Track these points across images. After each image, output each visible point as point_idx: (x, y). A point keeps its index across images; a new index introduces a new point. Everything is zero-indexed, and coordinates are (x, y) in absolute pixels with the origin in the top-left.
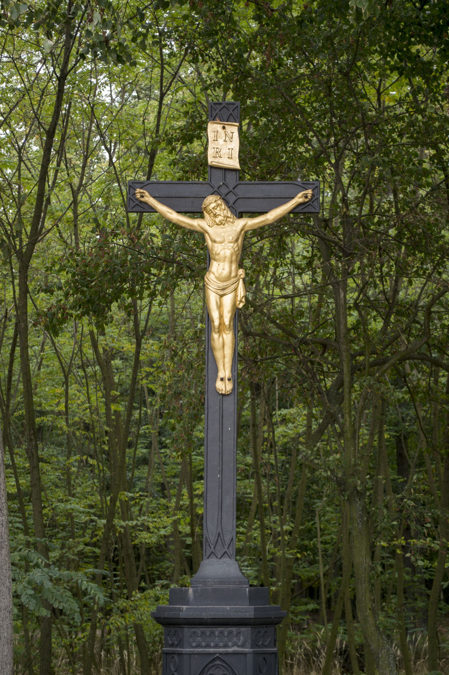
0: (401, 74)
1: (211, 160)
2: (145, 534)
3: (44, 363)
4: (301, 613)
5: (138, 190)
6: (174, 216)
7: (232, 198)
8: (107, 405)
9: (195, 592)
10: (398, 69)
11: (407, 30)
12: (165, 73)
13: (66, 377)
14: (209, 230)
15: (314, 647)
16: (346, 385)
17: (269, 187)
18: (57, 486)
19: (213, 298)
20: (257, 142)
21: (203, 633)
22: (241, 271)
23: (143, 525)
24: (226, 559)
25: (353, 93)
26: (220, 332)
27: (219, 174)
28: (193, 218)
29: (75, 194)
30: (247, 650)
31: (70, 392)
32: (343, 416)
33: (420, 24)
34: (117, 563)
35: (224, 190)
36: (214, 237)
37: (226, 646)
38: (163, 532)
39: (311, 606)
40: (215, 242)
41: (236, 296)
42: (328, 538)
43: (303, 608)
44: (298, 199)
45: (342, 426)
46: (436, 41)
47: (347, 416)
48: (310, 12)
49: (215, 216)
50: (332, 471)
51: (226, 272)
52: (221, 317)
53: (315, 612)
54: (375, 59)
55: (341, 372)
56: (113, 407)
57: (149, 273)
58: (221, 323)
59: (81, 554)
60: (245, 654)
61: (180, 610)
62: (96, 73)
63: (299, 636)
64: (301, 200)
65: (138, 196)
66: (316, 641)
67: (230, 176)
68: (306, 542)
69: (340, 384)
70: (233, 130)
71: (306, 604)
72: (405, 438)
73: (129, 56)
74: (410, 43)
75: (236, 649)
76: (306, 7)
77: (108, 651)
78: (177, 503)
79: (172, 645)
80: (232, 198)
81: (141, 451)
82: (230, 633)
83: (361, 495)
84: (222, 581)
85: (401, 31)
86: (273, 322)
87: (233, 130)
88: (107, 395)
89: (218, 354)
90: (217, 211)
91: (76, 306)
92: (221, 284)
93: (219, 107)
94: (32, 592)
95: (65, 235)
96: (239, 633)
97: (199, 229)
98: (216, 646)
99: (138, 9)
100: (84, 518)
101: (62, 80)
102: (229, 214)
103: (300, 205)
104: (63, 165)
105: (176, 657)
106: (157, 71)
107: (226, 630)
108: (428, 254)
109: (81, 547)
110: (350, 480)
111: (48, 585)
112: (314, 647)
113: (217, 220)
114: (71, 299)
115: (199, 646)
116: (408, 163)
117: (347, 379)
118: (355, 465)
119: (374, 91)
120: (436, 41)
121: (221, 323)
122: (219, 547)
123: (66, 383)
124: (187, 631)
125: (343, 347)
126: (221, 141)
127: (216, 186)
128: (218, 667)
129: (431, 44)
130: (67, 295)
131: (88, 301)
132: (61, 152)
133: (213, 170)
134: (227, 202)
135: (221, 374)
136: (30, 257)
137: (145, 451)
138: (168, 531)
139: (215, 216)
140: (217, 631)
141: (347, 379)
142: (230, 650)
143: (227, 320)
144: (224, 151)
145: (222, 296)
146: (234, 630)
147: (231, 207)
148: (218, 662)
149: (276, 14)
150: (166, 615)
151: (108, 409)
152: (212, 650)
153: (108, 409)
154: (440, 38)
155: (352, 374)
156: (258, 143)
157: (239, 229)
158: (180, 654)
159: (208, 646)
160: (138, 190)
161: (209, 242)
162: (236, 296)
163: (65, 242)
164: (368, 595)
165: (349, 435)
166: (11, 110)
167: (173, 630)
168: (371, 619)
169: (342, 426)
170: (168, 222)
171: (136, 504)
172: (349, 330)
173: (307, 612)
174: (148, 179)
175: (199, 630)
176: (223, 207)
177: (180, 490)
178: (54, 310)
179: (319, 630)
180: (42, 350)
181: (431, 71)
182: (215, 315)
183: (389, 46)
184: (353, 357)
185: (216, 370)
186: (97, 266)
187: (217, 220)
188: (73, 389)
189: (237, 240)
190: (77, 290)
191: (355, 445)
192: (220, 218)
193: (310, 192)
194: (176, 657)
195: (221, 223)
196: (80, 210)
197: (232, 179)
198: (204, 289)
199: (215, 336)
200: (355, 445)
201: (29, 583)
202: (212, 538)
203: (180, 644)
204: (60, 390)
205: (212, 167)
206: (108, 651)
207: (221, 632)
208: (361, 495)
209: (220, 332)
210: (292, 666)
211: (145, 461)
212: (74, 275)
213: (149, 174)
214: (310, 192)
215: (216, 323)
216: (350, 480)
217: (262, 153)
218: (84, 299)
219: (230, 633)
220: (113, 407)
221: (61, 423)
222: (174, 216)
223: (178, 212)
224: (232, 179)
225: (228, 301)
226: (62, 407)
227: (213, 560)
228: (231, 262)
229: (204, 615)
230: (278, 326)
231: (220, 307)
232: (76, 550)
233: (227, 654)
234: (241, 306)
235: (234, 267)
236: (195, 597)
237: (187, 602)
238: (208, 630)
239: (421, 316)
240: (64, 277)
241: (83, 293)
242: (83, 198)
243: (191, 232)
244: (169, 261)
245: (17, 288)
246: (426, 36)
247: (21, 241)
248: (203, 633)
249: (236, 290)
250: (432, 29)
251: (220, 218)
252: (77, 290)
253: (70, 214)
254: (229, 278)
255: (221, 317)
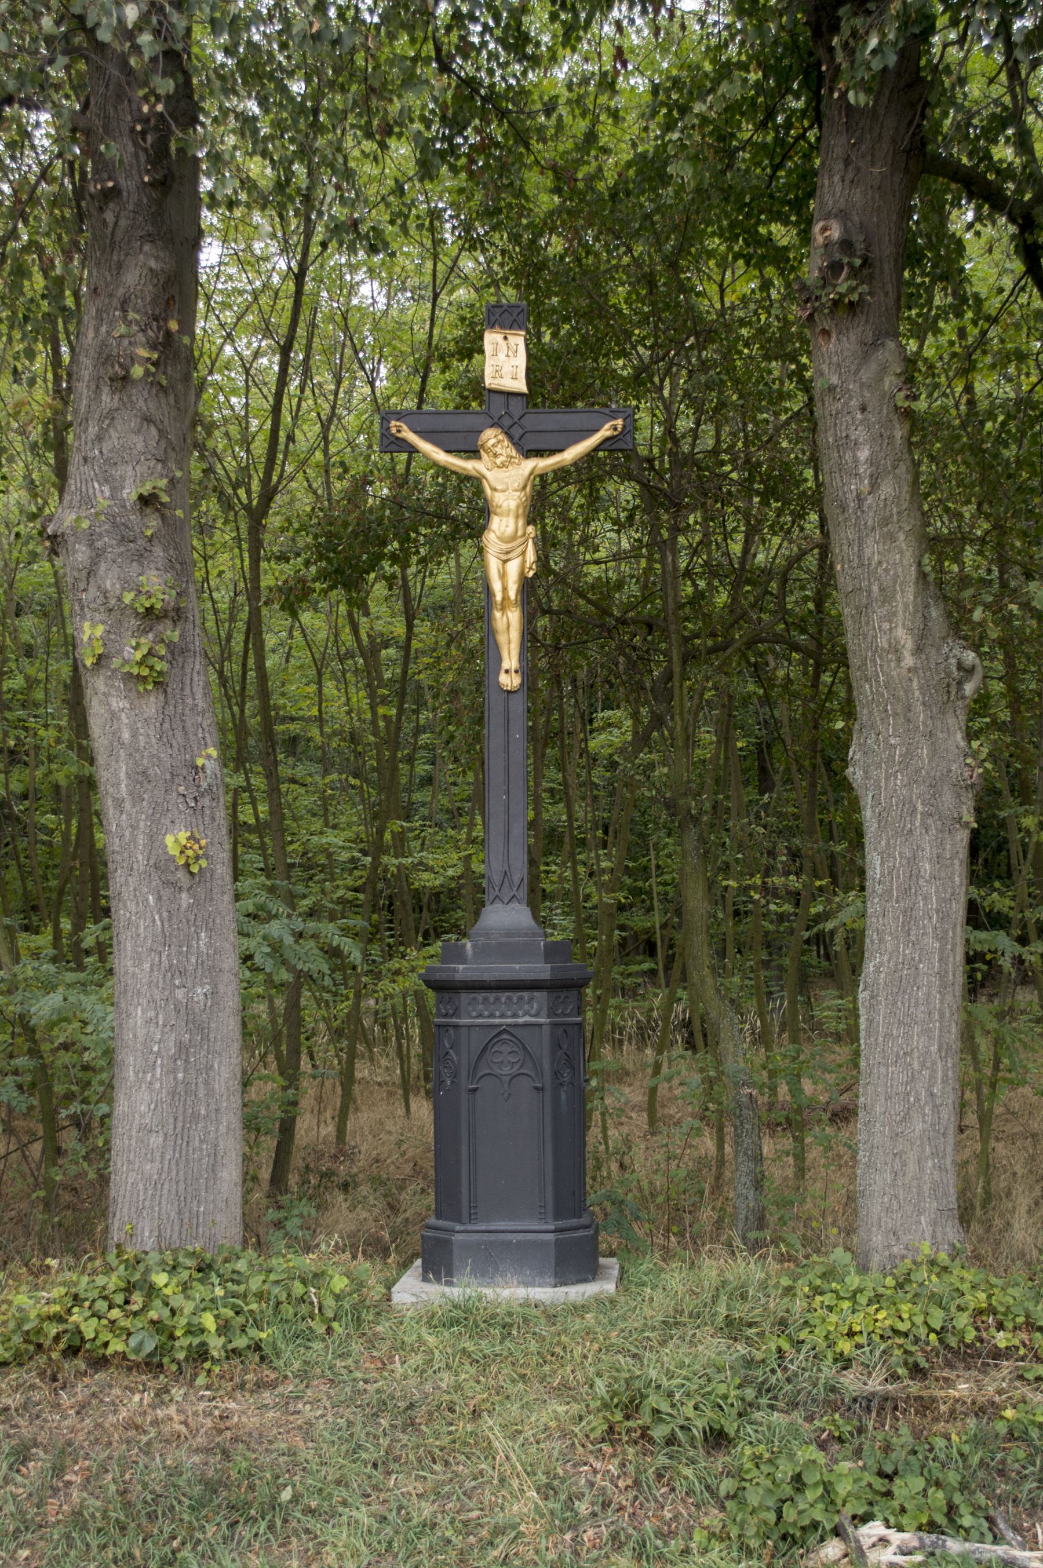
0: (748, 264)
1: (489, 382)
2: (425, 876)
3: (294, 652)
4: (637, 974)
5: (393, 423)
6: (441, 456)
7: (517, 432)
8: (373, 707)
9: (474, 947)
10: (743, 256)
11: (754, 204)
12: (440, 265)
13: (320, 674)
14: (488, 474)
15: (649, 1018)
16: (676, 677)
17: (566, 417)
18: (314, 815)
19: (493, 565)
20: (556, 356)
21: (486, 999)
22: (530, 529)
23: (421, 863)
24: (515, 905)
25: (685, 288)
26: (503, 609)
27: (501, 399)
28: (468, 458)
29: (325, 428)
30: (542, 1020)
31: (325, 691)
32: (672, 718)
33: (771, 196)
34: (392, 912)
35: (507, 422)
36: (494, 484)
37: (515, 1016)
38: (450, 872)
39: (646, 966)
40: (495, 490)
41: (524, 562)
42: (667, 877)
43: (635, 968)
44: (605, 432)
45: (671, 731)
46: (793, 218)
47: (677, 718)
48: (626, 182)
49: (496, 455)
50: (658, 792)
51: (510, 530)
52: (505, 589)
53: (653, 973)
54: (714, 243)
55: (670, 661)
56: (381, 711)
57: (419, 534)
58: (505, 598)
59: (341, 901)
60: (540, 1025)
61: (455, 970)
62: (353, 268)
63: (631, 1003)
64: (608, 433)
65: (394, 430)
66: (651, 1010)
67: (514, 402)
68: (640, 884)
69: (668, 676)
70: (518, 340)
71: (640, 963)
72: (769, 746)
73: (386, 245)
74: (759, 222)
75: (527, 1019)
76: (620, 175)
77: (384, 1026)
78: (469, 834)
79: (446, 1015)
80: (517, 432)
81: (422, 768)
82: (521, 998)
83: (696, 820)
84: (509, 933)
85: (746, 205)
86: (582, 595)
87: (518, 340)
88: (372, 696)
89: (502, 639)
90: (498, 450)
91: (322, 576)
92: (505, 547)
93: (499, 311)
94: (268, 950)
95: (315, 485)
96: (531, 999)
97: (474, 473)
98: (502, 1016)
99: (396, 180)
100: (345, 856)
101: (299, 278)
102: (514, 453)
103: (607, 439)
104: (308, 392)
105: (451, 1031)
106: (429, 265)
107: (515, 996)
108: (786, 503)
109: (341, 892)
110: (682, 802)
111: (289, 940)
112: (649, 1018)
113: (498, 461)
114: (313, 569)
115: (480, 1016)
116: (758, 382)
117: (677, 669)
118: (689, 782)
119: (715, 288)
120: (793, 218)
121: (505, 598)
122: (506, 889)
123: (319, 683)
124: (465, 997)
125: (673, 627)
126: (502, 356)
127: (496, 416)
128: (504, 1042)
129: (786, 223)
130: (307, 563)
131: (336, 571)
132: (307, 373)
133: (493, 396)
134: (510, 437)
135: (506, 665)
136: (264, 514)
137: (427, 767)
138: (459, 871)
139: (496, 455)
140: (504, 996)
141: (677, 669)
142: (521, 1020)
143: (512, 594)
144: (507, 370)
145: (505, 562)
146: (526, 995)
147: (517, 444)
148: (505, 1036)
149: (581, 185)
150: (438, 977)
151: (374, 713)
152: (497, 1021)
153: (374, 713)
154: (799, 214)
155: (684, 663)
156: (559, 358)
157: (527, 472)
158: (456, 1027)
159: (492, 1016)
160: (393, 423)
161: (488, 491)
162: (524, 562)
163: (315, 493)
164: (706, 948)
165: (680, 743)
166: (239, 319)
167: (446, 996)
168: (709, 980)
169: (671, 731)
170: (435, 464)
171: (417, 837)
172: (682, 606)
173: (644, 973)
174: (419, 407)
175: (480, 996)
176: (506, 443)
177: (473, 818)
178: (291, 583)
179: (656, 995)
180: (291, 636)
181: (788, 260)
182: (497, 586)
183: (732, 225)
184: (687, 640)
185: (500, 660)
186: (346, 525)
187: (498, 461)
188: (330, 687)
189: (524, 488)
190: (321, 557)
191: (688, 756)
192: (501, 459)
193: (619, 422)
194: (451, 1031)
195: (503, 465)
196: (332, 449)
197: (517, 407)
198: (481, 551)
199: (498, 614)
200: (688, 756)
201: (265, 938)
202: (497, 878)
203: (456, 1013)
204: (313, 688)
205: (490, 391)
206: (384, 1026)
207: (509, 998)
208: (696, 820)
209: (503, 609)
210: (621, 1042)
211: (428, 780)
212: (316, 537)
213: (421, 401)
214: (619, 422)
215: (499, 597)
216: (682, 802)
217: (565, 371)
218: (330, 569)
219: (521, 998)
220: (381, 711)
221: (314, 732)
222: (441, 456)
223: (448, 452)
224: (517, 407)
225: (513, 568)
226: (315, 712)
227: (498, 905)
228: (517, 517)
229: (486, 977)
230: (589, 601)
231: (503, 576)
232: (335, 896)
233: (516, 1025)
234: (531, 574)
235: (521, 523)
236: (475, 954)
237: (464, 961)
238: (491, 996)
239: (774, 585)
240: (305, 540)
241: (329, 560)
242: (339, 436)
243: (466, 478)
244: (442, 516)
245: (246, 555)
246: (779, 212)
247: (249, 492)
248: (486, 999)
249: (524, 553)
250: (789, 203)
251: (501, 459)
252: (321, 557)
253: (319, 455)
254: (514, 538)
255: (505, 589)
